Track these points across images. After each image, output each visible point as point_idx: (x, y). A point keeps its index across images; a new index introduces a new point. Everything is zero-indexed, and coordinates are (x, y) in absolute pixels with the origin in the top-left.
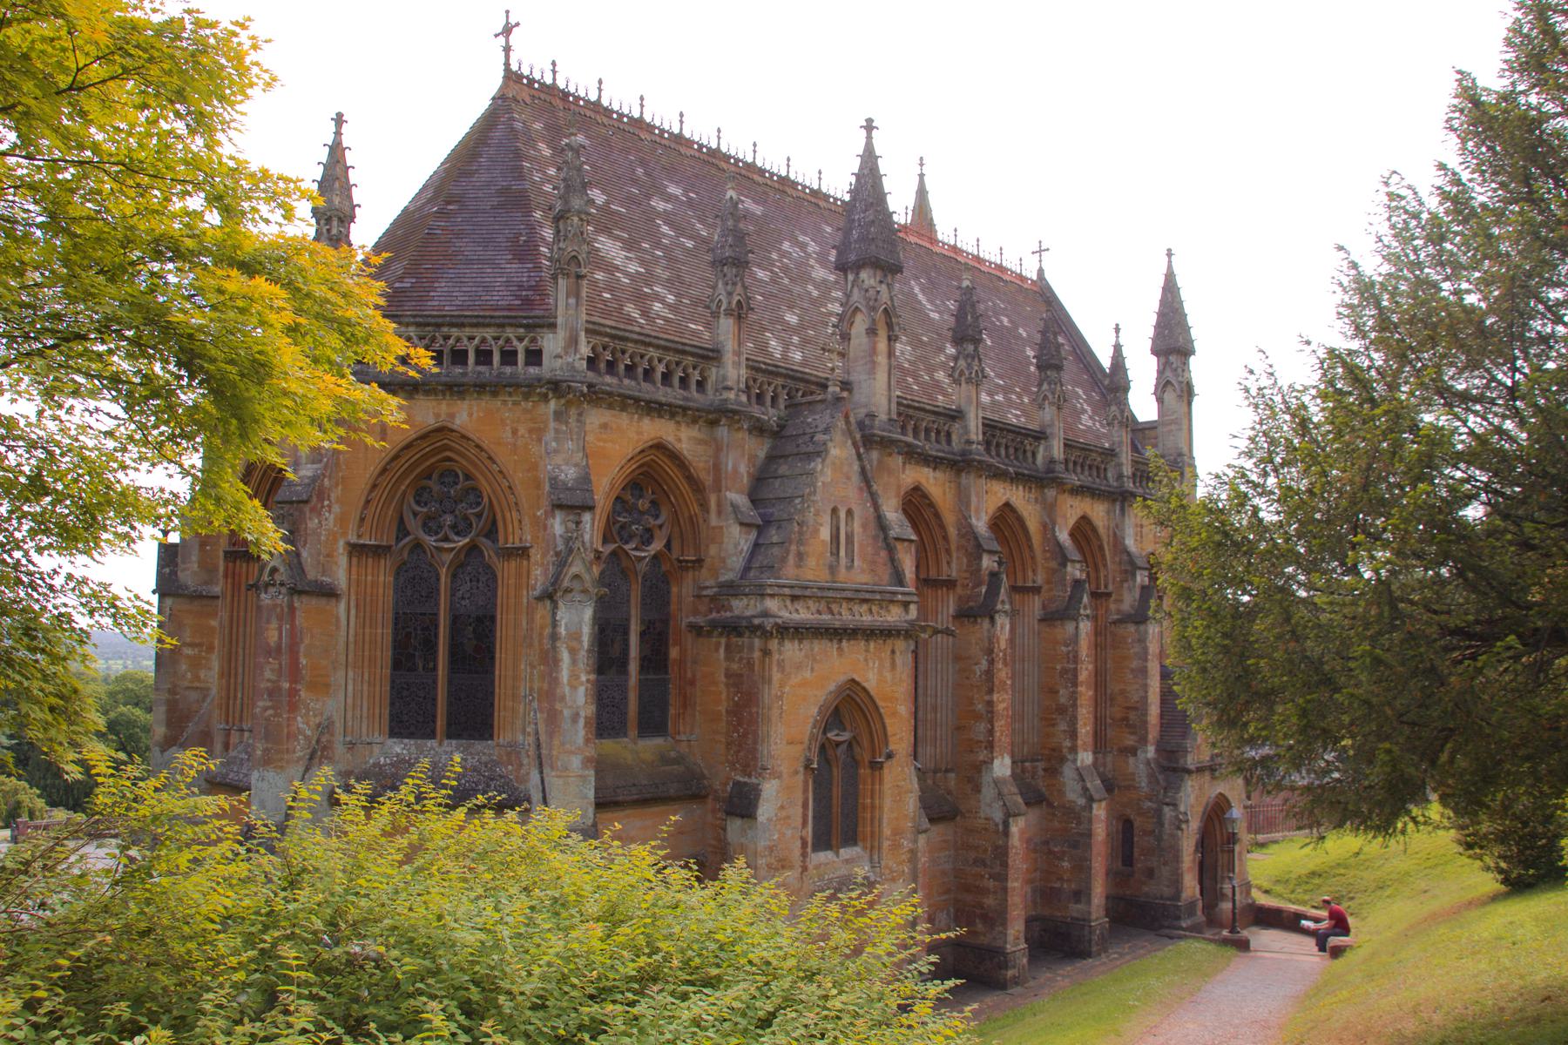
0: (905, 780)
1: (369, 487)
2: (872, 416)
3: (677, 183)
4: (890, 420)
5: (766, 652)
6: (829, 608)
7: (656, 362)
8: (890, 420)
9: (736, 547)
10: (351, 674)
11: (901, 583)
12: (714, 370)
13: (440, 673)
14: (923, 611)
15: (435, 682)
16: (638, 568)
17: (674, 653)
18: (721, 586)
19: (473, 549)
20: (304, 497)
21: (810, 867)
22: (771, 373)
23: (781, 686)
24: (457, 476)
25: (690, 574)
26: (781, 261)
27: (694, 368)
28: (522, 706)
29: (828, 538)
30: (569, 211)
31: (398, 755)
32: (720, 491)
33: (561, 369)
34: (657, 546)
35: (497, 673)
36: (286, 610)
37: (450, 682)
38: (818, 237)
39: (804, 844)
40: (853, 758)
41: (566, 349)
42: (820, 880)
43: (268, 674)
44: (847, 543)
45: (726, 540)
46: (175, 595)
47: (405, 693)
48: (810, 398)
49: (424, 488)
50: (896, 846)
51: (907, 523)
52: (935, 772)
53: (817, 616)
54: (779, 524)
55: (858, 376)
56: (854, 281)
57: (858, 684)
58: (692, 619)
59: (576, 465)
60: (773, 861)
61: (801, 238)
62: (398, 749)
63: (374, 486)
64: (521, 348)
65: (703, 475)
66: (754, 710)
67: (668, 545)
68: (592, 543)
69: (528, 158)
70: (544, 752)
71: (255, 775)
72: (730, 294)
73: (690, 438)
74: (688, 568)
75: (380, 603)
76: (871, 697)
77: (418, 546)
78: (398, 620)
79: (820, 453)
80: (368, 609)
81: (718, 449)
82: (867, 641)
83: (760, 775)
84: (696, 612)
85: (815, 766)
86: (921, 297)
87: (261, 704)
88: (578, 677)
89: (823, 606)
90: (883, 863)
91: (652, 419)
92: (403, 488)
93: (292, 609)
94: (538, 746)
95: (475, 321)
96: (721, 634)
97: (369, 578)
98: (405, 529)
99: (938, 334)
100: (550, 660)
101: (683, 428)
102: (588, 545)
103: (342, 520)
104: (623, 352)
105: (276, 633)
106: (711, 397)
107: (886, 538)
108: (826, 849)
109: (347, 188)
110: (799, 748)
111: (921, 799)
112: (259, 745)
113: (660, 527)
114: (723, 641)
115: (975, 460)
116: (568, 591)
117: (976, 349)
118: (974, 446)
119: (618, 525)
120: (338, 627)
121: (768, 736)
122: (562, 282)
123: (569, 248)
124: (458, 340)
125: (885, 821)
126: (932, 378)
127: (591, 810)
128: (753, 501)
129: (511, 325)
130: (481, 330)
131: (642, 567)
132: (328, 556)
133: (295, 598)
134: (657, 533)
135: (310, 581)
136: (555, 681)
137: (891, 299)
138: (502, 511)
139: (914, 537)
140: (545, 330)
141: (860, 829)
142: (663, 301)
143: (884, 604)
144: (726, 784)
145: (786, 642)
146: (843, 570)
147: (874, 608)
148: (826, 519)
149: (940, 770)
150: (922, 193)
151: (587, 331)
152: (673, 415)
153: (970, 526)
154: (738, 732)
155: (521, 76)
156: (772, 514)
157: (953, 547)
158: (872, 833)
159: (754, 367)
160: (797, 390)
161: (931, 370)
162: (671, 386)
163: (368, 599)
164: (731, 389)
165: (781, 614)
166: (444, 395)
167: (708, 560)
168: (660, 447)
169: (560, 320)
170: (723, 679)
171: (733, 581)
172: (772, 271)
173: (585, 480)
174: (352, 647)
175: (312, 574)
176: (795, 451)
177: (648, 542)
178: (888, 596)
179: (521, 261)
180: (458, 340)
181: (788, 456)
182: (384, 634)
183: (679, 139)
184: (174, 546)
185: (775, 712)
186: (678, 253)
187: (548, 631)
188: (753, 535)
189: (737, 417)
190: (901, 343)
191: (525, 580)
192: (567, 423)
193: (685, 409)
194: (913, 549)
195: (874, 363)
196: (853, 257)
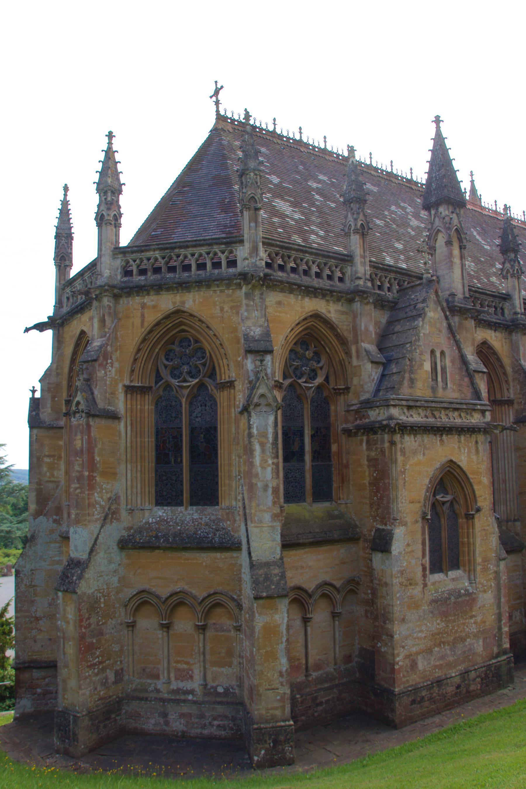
0: (489, 525)
1: (135, 350)
2: (453, 295)
3: (325, 174)
4: (465, 298)
5: (393, 443)
6: (433, 414)
7: (311, 263)
8: (465, 298)
9: (369, 377)
10: (129, 466)
11: (479, 398)
12: (349, 268)
13: (184, 464)
14: (493, 419)
15: (182, 470)
16: (308, 394)
17: (334, 448)
18: (361, 403)
19: (201, 386)
20: (95, 358)
21: (429, 584)
22: (386, 270)
23: (404, 465)
24: (190, 341)
25: (342, 397)
26: (391, 216)
27: (336, 267)
28: (234, 483)
29: (430, 369)
30: (247, 170)
31: (160, 516)
32: (357, 343)
33: (248, 266)
34: (319, 380)
35: (219, 463)
36: (85, 427)
37: (191, 471)
38: (412, 203)
39: (424, 569)
40: (454, 512)
41: (250, 254)
42: (436, 592)
43: (77, 468)
44: (442, 373)
45: (363, 373)
46: (39, 427)
47: (164, 478)
48: (412, 284)
49: (170, 350)
50: (485, 569)
51: (480, 361)
52: (507, 521)
53: (425, 419)
54: (397, 361)
55: (442, 271)
56: (435, 213)
57: (455, 463)
58: (344, 426)
59: (261, 326)
60: (403, 580)
61: (402, 204)
62: (160, 513)
63: (139, 350)
64: (223, 257)
65: (346, 334)
66: (387, 481)
67: (327, 379)
68: (274, 374)
69: (230, 159)
70: (247, 511)
71: (72, 530)
72: (356, 220)
73: (336, 311)
74: (340, 394)
75: (146, 422)
76: (464, 472)
77: (168, 386)
78: (158, 433)
79: (421, 314)
80: (139, 426)
81: (355, 317)
82: (459, 435)
83: (392, 523)
84: (347, 421)
85: (429, 517)
86: (478, 237)
87: (73, 486)
88: (266, 461)
89: (428, 413)
90: (477, 580)
91: (311, 298)
92: (157, 350)
93: (89, 426)
94: (244, 508)
95: (194, 243)
96: (363, 434)
97: (139, 407)
98: (160, 376)
99: (491, 258)
100: (249, 451)
101: (331, 304)
102: (270, 376)
103: (120, 371)
104: (289, 257)
105: (80, 442)
106: (348, 285)
107: (467, 370)
108: (439, 572)
109: (116, 174)
110: (418, 505)
111: (500, 538)
112: (73, 511)
113: (321, 368)
114: (365, 438)
115: (521, 324)
116: (257, 405)
117: (516, 256)
118: (519, 316)
119: (293, 367)
120: (120, 438)
121: (397, 498)
122: (246, 214)
123: (249, 192)
124: (186, 257)
125: (477, 552)
126: (489, 281)
127: (279, 549)
128: (380, 350)
129: (217, 244)
130: (199, 248)
131: (310, 394)
132: (112, 393)
133: (90, 419)
134: (319, 372)
135: (100, 409)
136: (251, 464)
137: (460, 223)
138: (218, 360)
139: (485, 370)
140: (238, 245)
141: (461, 558)
142: (317, 234)
143: (469, 411)
144: (371, 531)
145: (406, 436)
146: (440, 390)
147: (463, 415)
148: (427, 357)
149: (510, 521)
150: (472, 182)
151: (264, 243)
152: (324, 296)
153: (520, 365)
154: (377, 496)
155: (227, 118)
156: (392, 356)
157: (510, 379)
158: (469, 561)
159: (374, 266)
160: (404, 281)
161: (488, 276)
162: (322, 278)
163: (139, 419)
164: (360, 278)
165: (400, 418)
166: (178, 290)
167: (353, 388)
168: (316, 316)
169: (246, 237)
170: (366, 462)
171: (369, 399)
172: (385, 221)
173: (267, 335)
174: (129, 450)
175: (101, 405)
176: (405, 316)
177: (314, 377)
178: (471, 407)
179: (226, 212)
180: (186, 257)
181: (400, 320)
182: (150, 441)
183: (324, 151)
184: (38, 399)
185: (400, 482)
186: (326, 210)
187: (246, 432)
188: (380, 369)
189: (365, 295)
190: (468, 261)
191: (232, 402)
192: (253, 300)
193: (331, 292)
194: (485, 378)
195: (451, 262)
196: (433, 199)
